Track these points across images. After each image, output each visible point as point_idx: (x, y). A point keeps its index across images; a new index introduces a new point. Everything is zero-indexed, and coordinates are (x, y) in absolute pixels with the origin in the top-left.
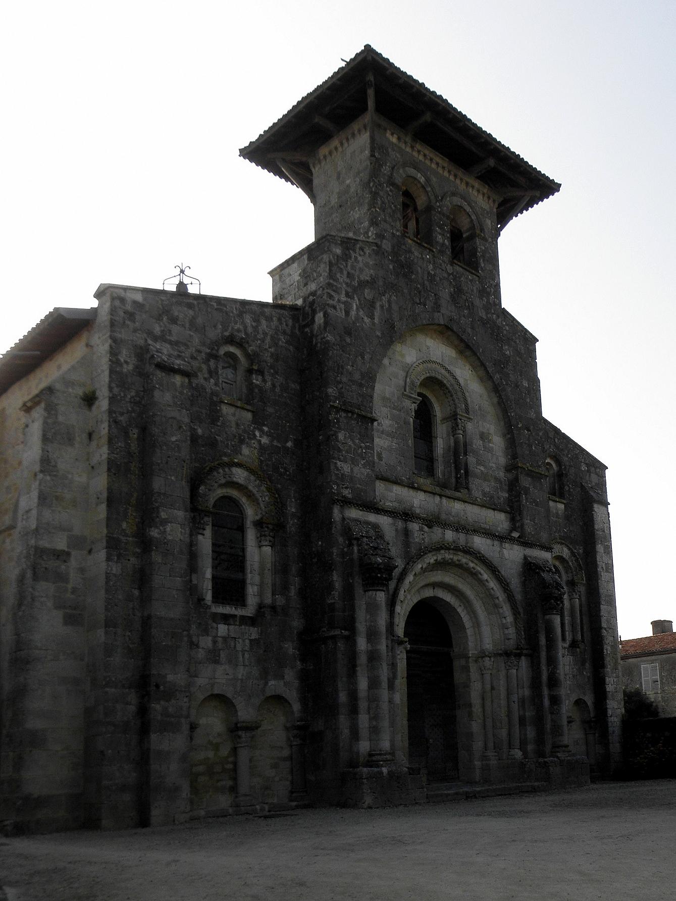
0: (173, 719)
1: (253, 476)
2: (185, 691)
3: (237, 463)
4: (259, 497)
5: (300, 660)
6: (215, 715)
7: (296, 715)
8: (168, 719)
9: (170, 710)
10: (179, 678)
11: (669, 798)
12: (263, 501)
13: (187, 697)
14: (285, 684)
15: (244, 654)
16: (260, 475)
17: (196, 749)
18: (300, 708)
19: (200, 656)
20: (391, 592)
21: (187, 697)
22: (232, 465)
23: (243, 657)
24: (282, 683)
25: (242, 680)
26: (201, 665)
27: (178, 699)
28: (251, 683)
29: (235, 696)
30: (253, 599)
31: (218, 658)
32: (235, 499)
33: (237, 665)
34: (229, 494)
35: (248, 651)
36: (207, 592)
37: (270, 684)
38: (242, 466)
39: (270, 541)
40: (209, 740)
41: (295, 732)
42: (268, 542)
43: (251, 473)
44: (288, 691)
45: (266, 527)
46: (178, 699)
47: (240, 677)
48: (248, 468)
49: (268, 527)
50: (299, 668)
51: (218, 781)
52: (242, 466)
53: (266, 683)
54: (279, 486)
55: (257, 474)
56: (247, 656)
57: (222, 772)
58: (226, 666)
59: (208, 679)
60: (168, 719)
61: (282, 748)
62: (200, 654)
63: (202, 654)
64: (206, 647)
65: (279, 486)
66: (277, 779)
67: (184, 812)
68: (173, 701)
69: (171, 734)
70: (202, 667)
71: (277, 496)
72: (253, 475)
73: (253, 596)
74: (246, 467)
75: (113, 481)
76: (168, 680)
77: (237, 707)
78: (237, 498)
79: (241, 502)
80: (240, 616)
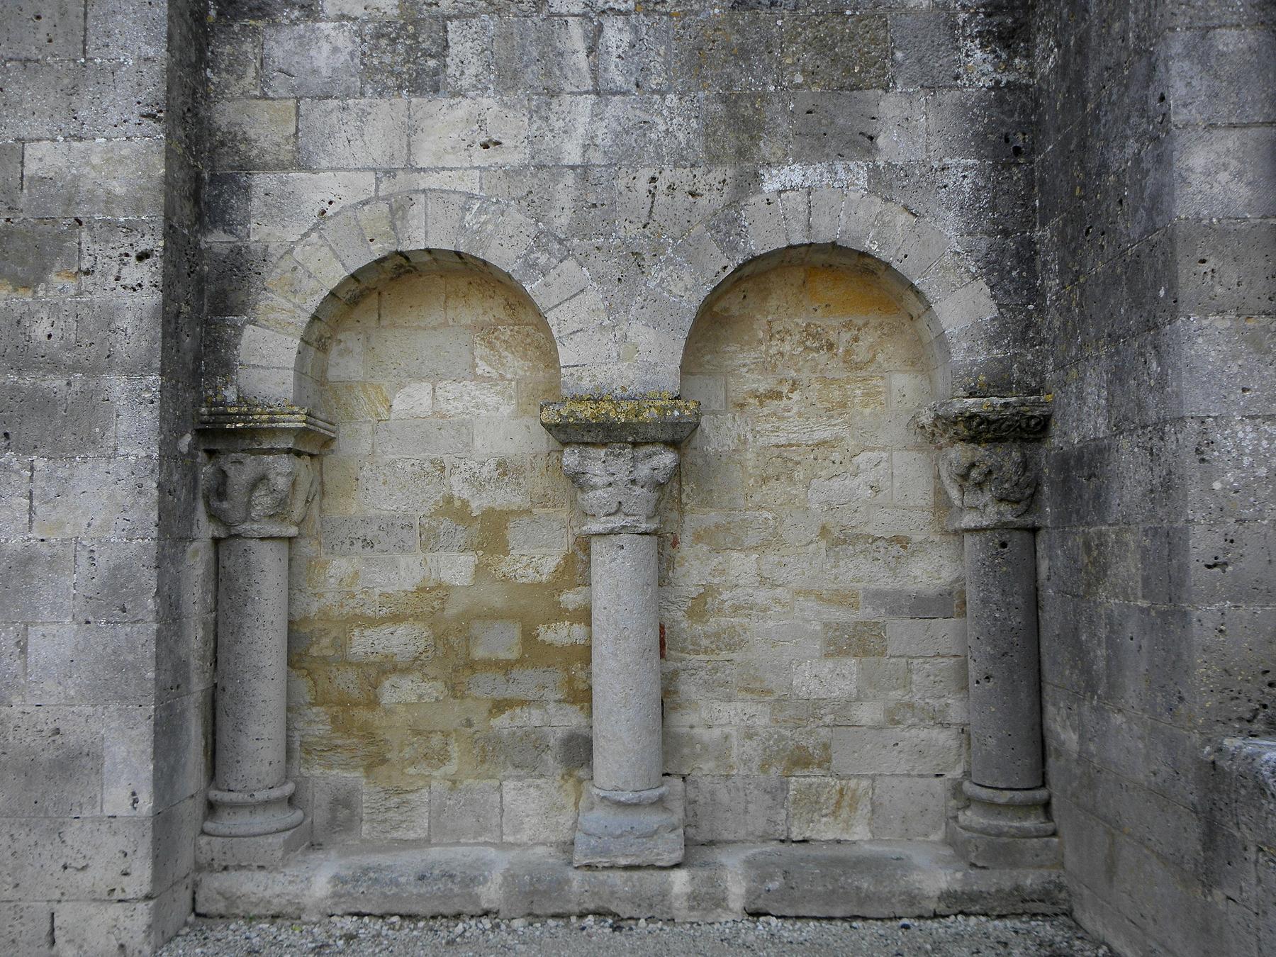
0: (56, 383)
2: (130, 228)
5: (986, 39)
6: (482, 368)
7: (958, 357)
8: (28, 381)
9: (40, 330)
10: (96, 160)
13: (142, 257)
14: (880, 182)
15: (600, 29)
17: (368, 544)
18: (987, 309)
19: (322, 57)
21: (142, 257)
23: (591, 50)
24: (857, 174)
25: (583, 171)
26: (332, 103)
27: (87, 273)
28: (643, 185)
29: (543, 259)
31: (432, 63)
33: (553, 93)
35: (626, 14)
37: (770, 186)
40: (449, 500)
41: (960, 453)
44: (903, 218)
46: (87, 273)
47: (572, 155)
50: (986, 82)
51: (500, 706)
53: (749, 182)
56: (615, 36)
57: (520, 661)
58: (486, 102)
59: (370, 177)
60: (28, 381)
61: (902, 541)
62: (326, 48)
63: (335, 50)
64: (359, 11)
66: (867, 713)
67: (112, 896)
68: (59, 283)
69: (40, 464)
70: (334, 118)
75: (1246, 83)
76: (31, 168)
77: (551, 317)
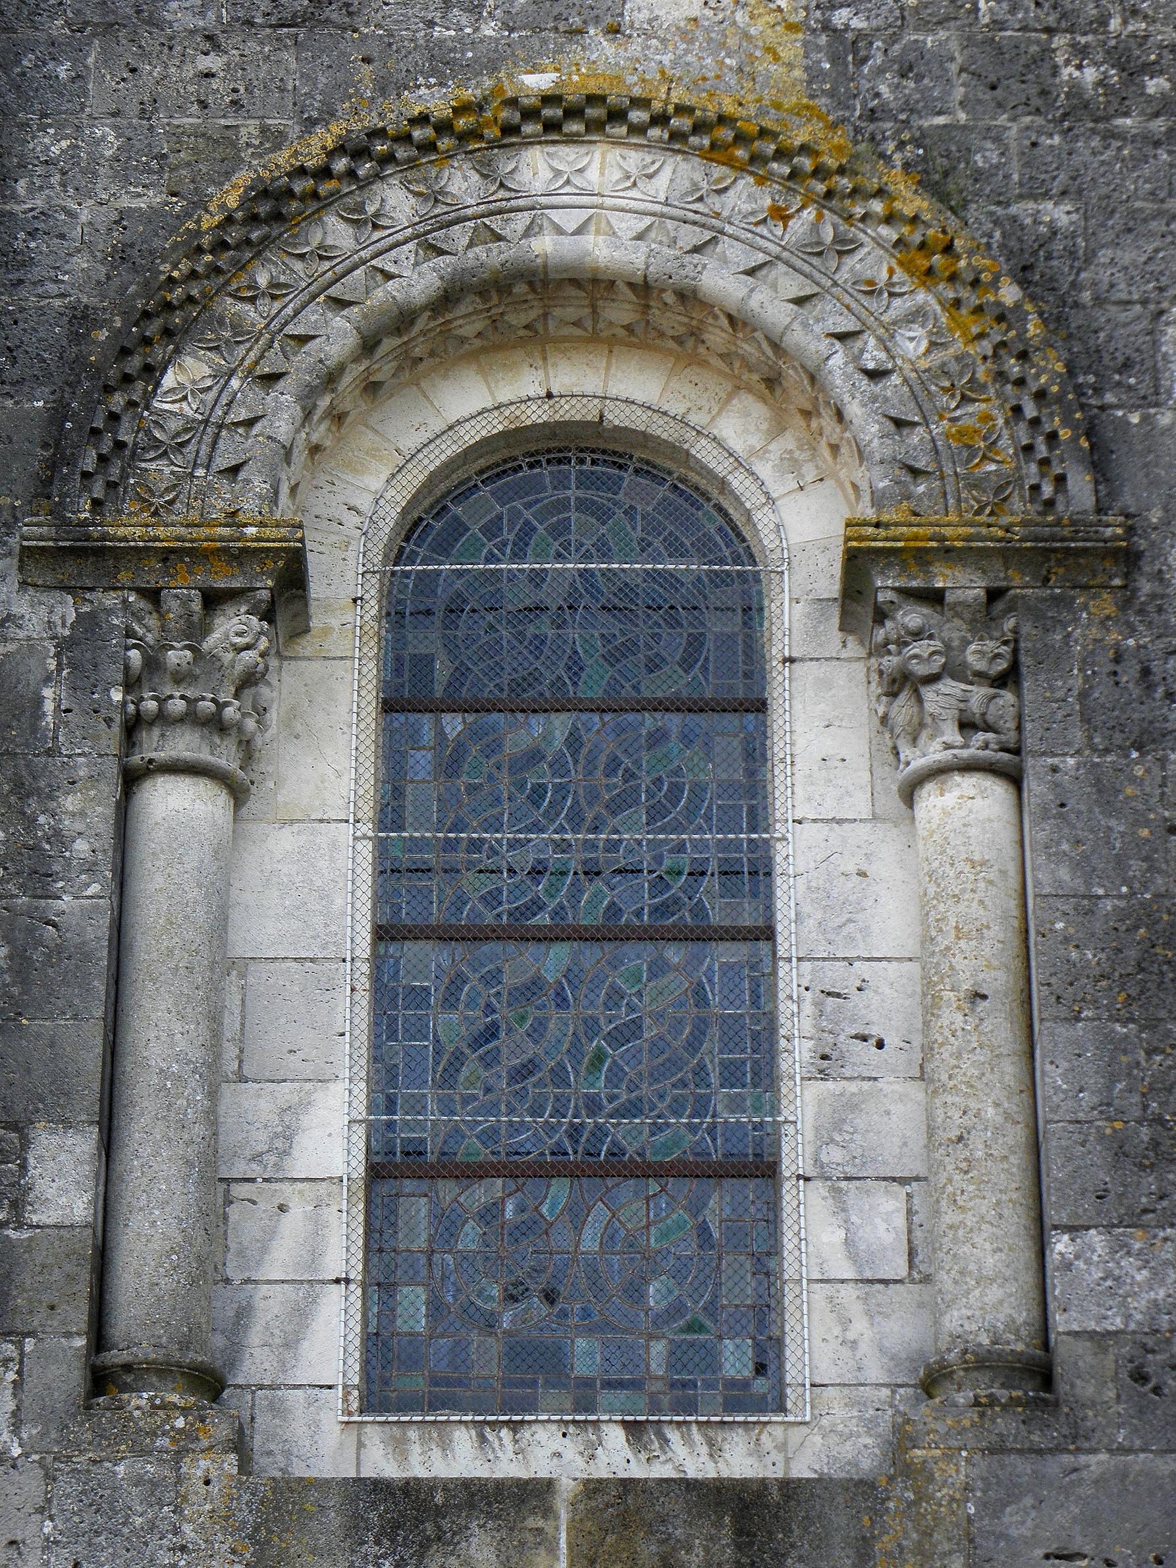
1: (746, 183)
3: (549, 99)
4: (824, 345)
11: (697, 1359)
12: (875, 375)
16: (804, 149)
20: (504, 141)
22: (510, 130)
30: (860, 1327)
32: (645, 438)
34: (568, 411)
36: (301, 1315)
38: (617, 115)
39: (966, 725)
42: (952, 734)
43: (716, 153)
45: (908, 594)
48: (680, 123)
49: (934, 598)
52: (617, 115)
54: (1060, 214)
55: (782, 154)
65: (1060, 214)
71: (1009, 293)
72: (741, 169)
73: (848, 1294)
74: (660, 120)
78: (662, 430)
79: (704, 452)
80: (593, 1488)
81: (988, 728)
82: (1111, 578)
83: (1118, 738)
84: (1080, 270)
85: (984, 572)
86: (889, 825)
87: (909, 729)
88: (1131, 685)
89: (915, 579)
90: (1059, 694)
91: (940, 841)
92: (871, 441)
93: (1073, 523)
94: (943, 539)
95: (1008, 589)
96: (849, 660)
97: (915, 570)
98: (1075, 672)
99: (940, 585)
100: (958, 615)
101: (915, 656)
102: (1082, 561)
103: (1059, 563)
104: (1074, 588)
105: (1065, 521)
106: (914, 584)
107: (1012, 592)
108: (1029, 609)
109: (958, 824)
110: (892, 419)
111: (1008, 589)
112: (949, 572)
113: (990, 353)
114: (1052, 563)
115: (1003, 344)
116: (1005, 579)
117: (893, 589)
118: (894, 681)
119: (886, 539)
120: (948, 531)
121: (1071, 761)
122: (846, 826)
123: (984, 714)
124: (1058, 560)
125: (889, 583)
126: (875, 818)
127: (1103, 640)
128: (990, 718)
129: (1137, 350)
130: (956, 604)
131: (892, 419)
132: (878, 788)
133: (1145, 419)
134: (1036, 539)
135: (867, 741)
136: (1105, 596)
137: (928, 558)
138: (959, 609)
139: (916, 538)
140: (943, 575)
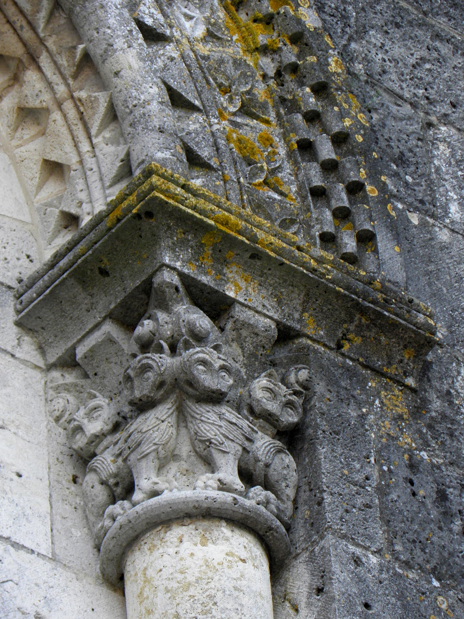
81: (267, 486)
82: (406, 374)
83: (419, 557)
84: (351, 39)
85: (279, 302)
86: (70, 574)
87: (162, 453)
88: (428, 502)
89: (206, 274)
90: (359, 477)
91: (203, 599)
92: (147, 102)
93: (384, 290)
94: (254, 239)
95: (299, 335)
96: (24, 362)
97: (208, 262)
98: (372, 459)
99: (231, 294)
100: (240, 340)
101: (204, 362)
102: (383, 338)
103: (360, 330)
104: (366, 367)
105: (377, 285)
106: (204, 279)
107: (304, 341)
108: (321, 367)
109: (229, 585)
110: (170, 89)
111: (299, 335)
112: (243, 284)
113: (271, 72)
114: (352, 328)
115: (294, 68)
116: (300, 321)
117: (181, 275)
118: (161, 384)
119: (194, 208)
120: (261, 235)
121: (374, 560)
122: (22, 553)
123: (267, 466)
124: (359, 326)
125: (178, 265)
126: (54, 559)
127: (397, 438)
128: (273, 474)
129: (411, 150)
130: (246, 325)
131: (170, 89)
132: (58, 526)
133: (423, 224)
134: (347, 288)
135: (45, 465)
136: (397, 392)
137: (230, 254)
138: (244, 333)
139: (226, 223)
140: (236, 285)
